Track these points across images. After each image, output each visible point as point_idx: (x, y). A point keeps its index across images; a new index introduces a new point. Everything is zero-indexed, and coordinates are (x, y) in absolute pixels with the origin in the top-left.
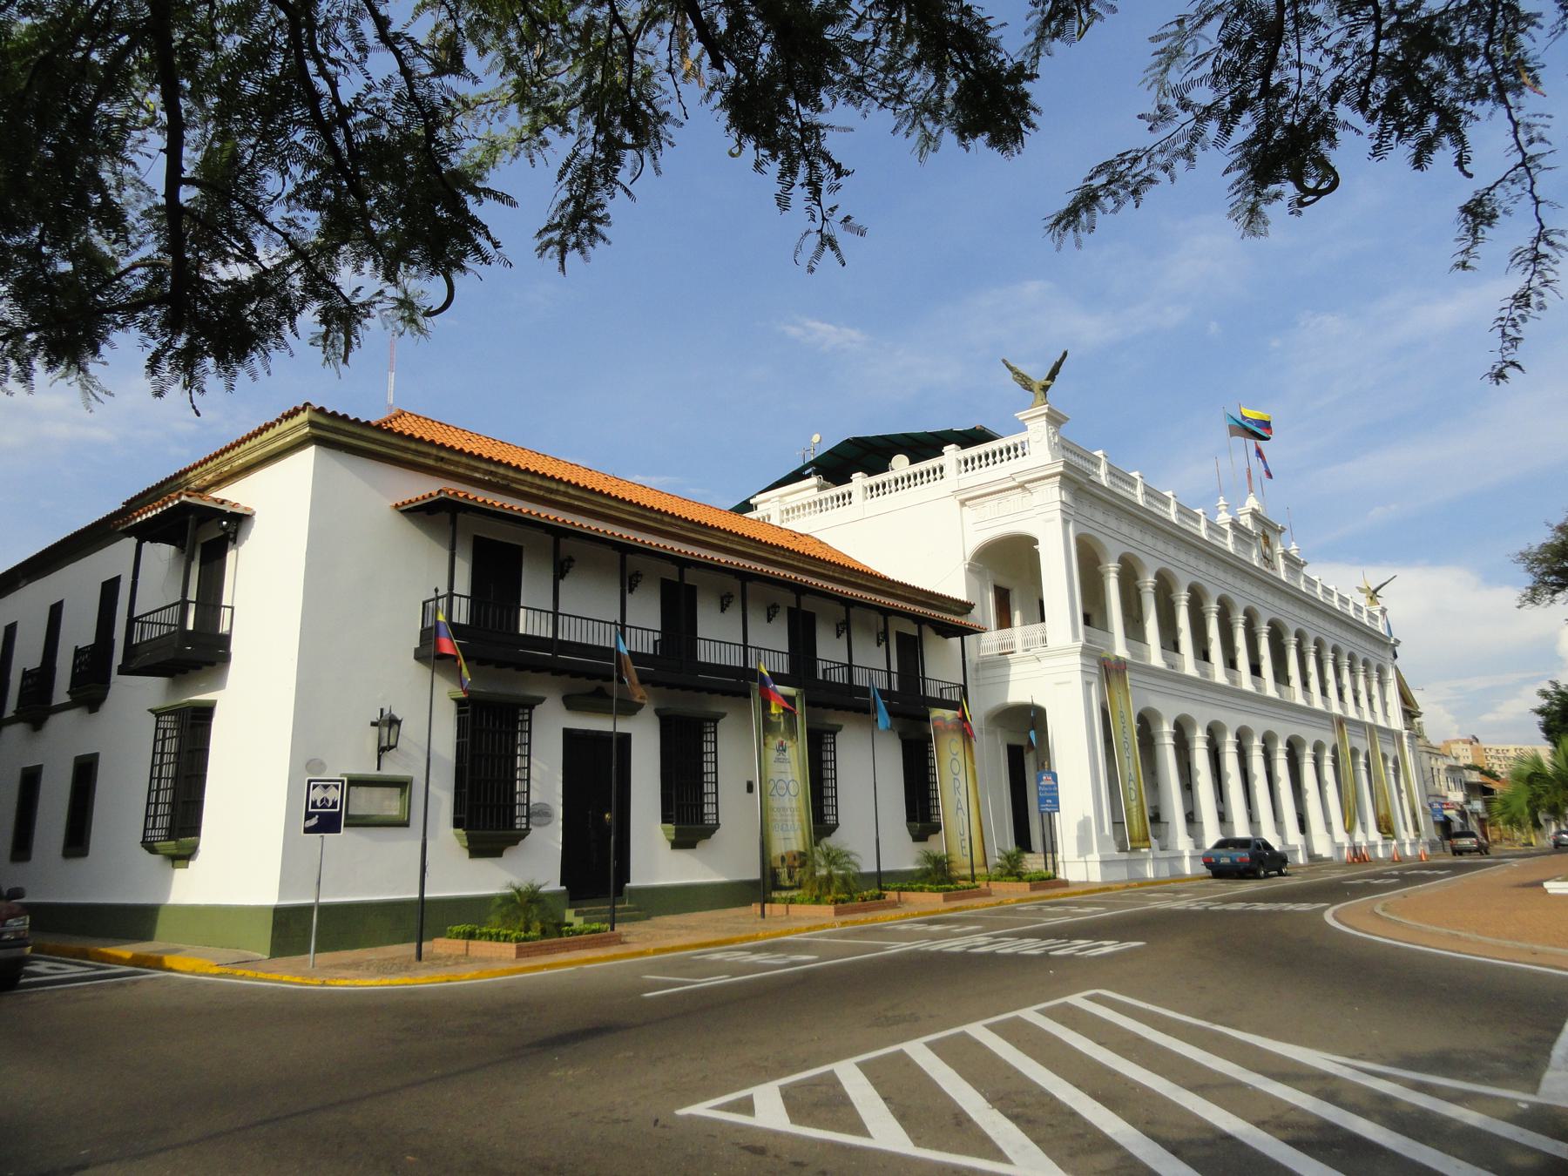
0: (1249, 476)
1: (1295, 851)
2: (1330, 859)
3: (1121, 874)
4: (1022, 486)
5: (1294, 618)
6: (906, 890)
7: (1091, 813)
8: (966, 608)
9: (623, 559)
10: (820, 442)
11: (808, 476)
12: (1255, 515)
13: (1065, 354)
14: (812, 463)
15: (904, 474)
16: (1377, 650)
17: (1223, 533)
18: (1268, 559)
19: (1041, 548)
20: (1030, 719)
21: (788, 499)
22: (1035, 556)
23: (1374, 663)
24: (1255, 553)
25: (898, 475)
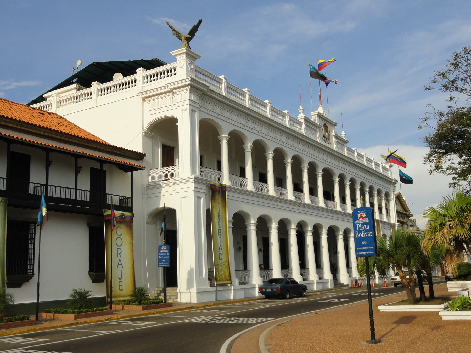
0: (320, 97)
1: (312, 283)
2: (347, 285)
3: (211, 298)
4: (171, 91)
5: (338, 169)
6: (59, 312)
7: (194, 266)
8: (140, 156)
9: (47, 155)
10: (80, 64)
11: (73, 83)
12: (319, 115)
13: (200, 22)
14: (74, 76)
15: (120, 82)
16: (386, 185)
17: (300, 124)
18: (327, 139)
19: (179, 124)
20: (168, 216)
21: (62, 95)
22: (176, 129)
23: (384, 191)
24: (318, 134)
25: (117, 83)
